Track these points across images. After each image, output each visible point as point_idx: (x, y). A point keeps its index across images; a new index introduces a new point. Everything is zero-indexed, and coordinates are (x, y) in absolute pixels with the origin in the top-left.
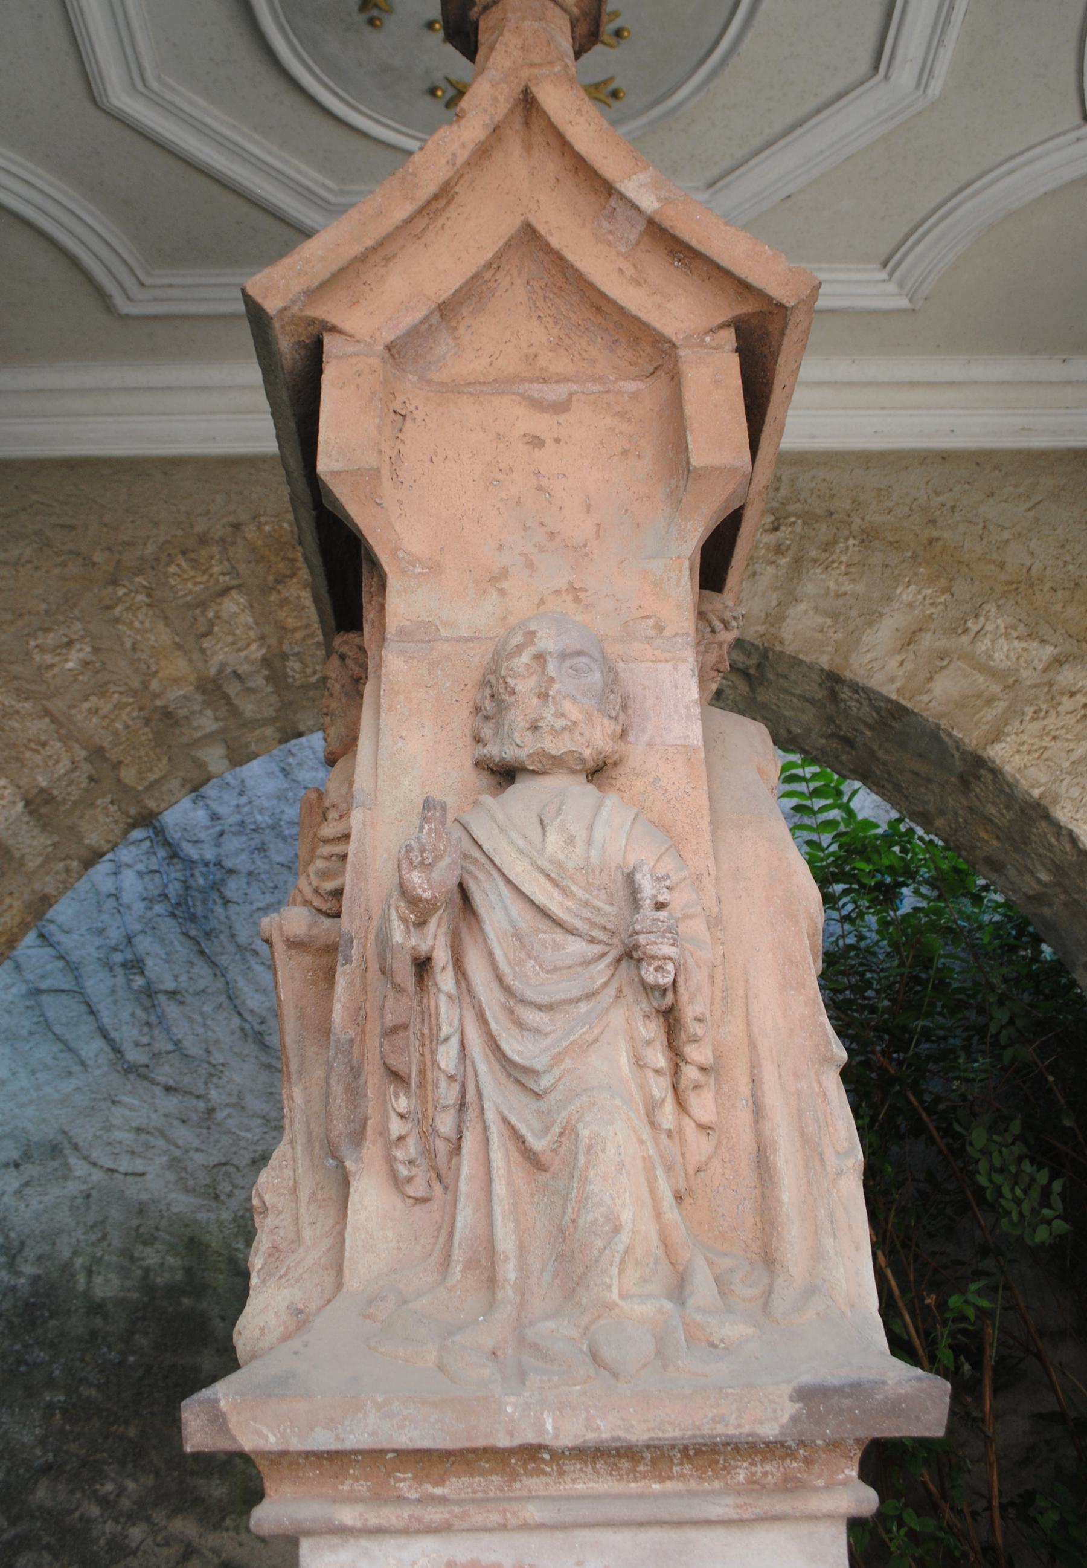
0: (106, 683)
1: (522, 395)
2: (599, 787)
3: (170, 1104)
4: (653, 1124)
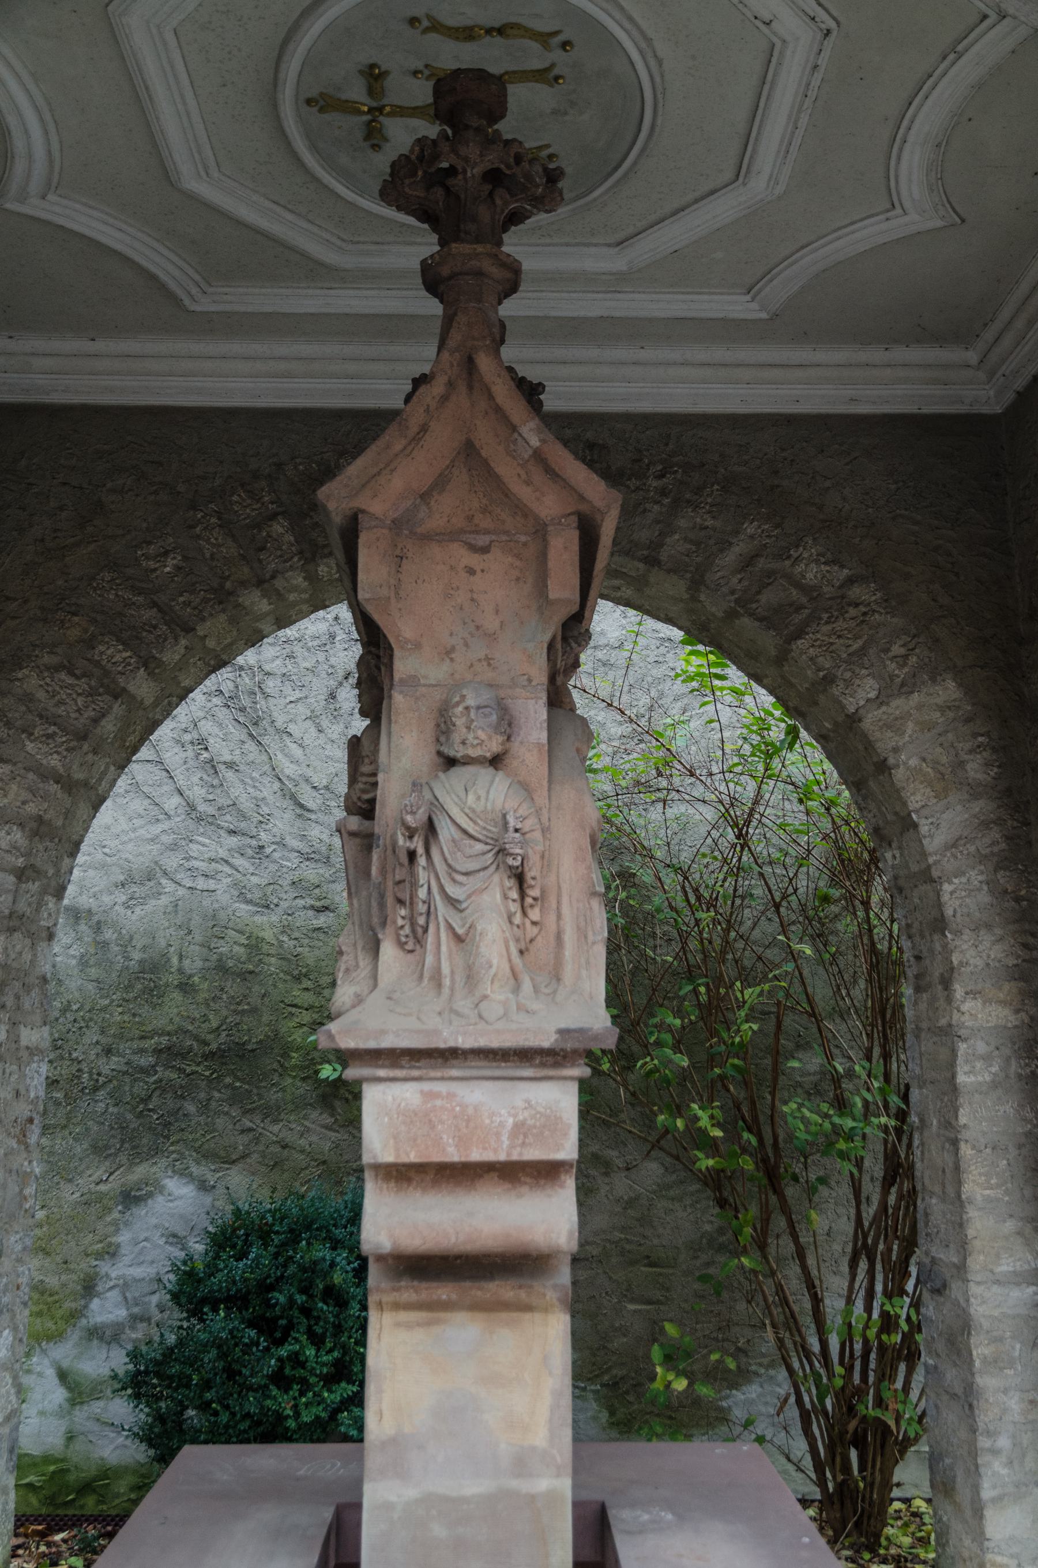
0: (194, 584)
1: (466, 543)
2: (496, 769)
3: (233, 841)
4: (511, 922)
